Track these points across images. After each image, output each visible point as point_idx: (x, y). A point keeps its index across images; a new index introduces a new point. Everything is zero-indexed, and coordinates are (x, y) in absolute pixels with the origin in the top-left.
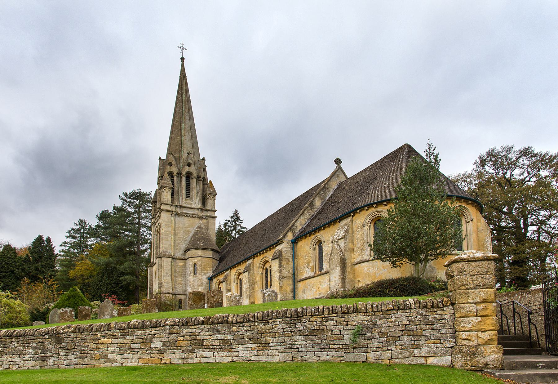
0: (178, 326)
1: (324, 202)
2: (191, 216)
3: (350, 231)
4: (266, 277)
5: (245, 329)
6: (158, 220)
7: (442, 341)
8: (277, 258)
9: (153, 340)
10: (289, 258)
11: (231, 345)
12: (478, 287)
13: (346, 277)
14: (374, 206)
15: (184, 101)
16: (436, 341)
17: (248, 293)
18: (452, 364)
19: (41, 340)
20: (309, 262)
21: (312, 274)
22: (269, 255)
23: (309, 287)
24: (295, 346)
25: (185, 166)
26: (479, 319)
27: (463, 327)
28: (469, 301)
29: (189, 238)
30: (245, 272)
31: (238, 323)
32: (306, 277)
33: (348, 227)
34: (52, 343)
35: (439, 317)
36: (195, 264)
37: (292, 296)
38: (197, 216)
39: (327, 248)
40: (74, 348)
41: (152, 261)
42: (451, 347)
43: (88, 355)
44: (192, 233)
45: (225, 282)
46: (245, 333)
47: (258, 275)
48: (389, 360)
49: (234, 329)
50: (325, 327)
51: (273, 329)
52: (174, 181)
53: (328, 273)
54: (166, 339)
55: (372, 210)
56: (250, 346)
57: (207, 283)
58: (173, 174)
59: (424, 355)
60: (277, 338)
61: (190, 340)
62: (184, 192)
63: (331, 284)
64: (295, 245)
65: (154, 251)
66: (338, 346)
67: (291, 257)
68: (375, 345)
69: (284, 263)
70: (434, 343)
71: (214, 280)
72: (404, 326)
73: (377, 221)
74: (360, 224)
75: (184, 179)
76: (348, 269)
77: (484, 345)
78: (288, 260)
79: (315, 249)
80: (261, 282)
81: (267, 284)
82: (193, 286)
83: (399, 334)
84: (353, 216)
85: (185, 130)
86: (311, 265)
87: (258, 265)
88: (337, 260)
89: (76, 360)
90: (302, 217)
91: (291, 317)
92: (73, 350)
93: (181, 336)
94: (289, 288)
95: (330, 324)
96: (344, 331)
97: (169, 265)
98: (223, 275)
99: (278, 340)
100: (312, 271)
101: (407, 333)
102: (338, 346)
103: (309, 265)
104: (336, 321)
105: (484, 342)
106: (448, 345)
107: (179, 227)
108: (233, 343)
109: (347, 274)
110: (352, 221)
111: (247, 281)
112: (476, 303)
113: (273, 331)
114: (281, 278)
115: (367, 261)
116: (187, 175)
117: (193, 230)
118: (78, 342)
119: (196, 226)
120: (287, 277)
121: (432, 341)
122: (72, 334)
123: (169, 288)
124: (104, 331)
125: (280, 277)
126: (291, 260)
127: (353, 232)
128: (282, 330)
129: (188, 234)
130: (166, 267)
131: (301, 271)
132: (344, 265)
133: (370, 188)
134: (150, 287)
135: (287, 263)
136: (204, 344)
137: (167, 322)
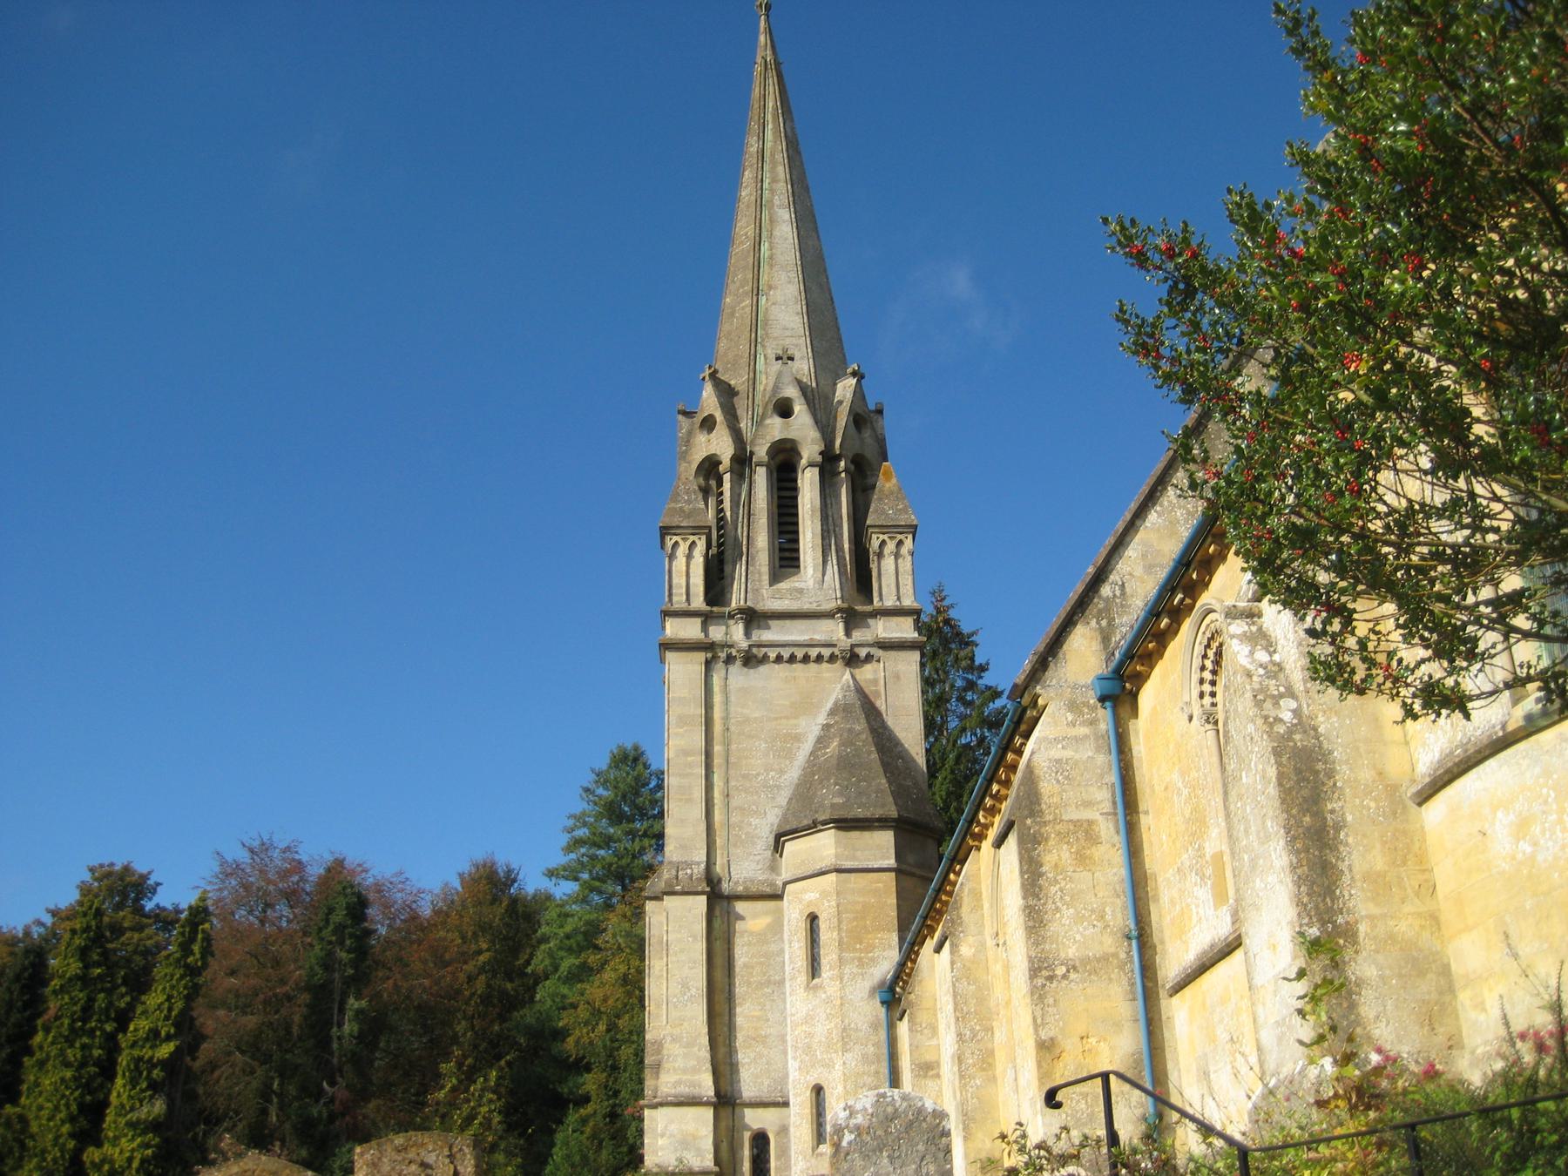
2: (800, 653)
10: (1086, 814)
13: (1350, 933)
15: (767, 154)
25: (763, 417)
29: (793, 773)
36: (813, 919)
38: (826, 652)
44: (807, 746)
57: (875, 1027)
64: (1124, 711)
67: (1107, 806)
69: (1055, 855)
75: (761, 477)
78: (1087, 831)
85: (771, 266)
90: (1153, 517)
97: (695, 937)
107: (747, 720)
109: (1359, 903)
116: (780, 457)
117: (811, 727)
119: (829, 705)
120: (1090, 966)
123: (695, 1070)
130: (682, 951)
132: (1319, 815)
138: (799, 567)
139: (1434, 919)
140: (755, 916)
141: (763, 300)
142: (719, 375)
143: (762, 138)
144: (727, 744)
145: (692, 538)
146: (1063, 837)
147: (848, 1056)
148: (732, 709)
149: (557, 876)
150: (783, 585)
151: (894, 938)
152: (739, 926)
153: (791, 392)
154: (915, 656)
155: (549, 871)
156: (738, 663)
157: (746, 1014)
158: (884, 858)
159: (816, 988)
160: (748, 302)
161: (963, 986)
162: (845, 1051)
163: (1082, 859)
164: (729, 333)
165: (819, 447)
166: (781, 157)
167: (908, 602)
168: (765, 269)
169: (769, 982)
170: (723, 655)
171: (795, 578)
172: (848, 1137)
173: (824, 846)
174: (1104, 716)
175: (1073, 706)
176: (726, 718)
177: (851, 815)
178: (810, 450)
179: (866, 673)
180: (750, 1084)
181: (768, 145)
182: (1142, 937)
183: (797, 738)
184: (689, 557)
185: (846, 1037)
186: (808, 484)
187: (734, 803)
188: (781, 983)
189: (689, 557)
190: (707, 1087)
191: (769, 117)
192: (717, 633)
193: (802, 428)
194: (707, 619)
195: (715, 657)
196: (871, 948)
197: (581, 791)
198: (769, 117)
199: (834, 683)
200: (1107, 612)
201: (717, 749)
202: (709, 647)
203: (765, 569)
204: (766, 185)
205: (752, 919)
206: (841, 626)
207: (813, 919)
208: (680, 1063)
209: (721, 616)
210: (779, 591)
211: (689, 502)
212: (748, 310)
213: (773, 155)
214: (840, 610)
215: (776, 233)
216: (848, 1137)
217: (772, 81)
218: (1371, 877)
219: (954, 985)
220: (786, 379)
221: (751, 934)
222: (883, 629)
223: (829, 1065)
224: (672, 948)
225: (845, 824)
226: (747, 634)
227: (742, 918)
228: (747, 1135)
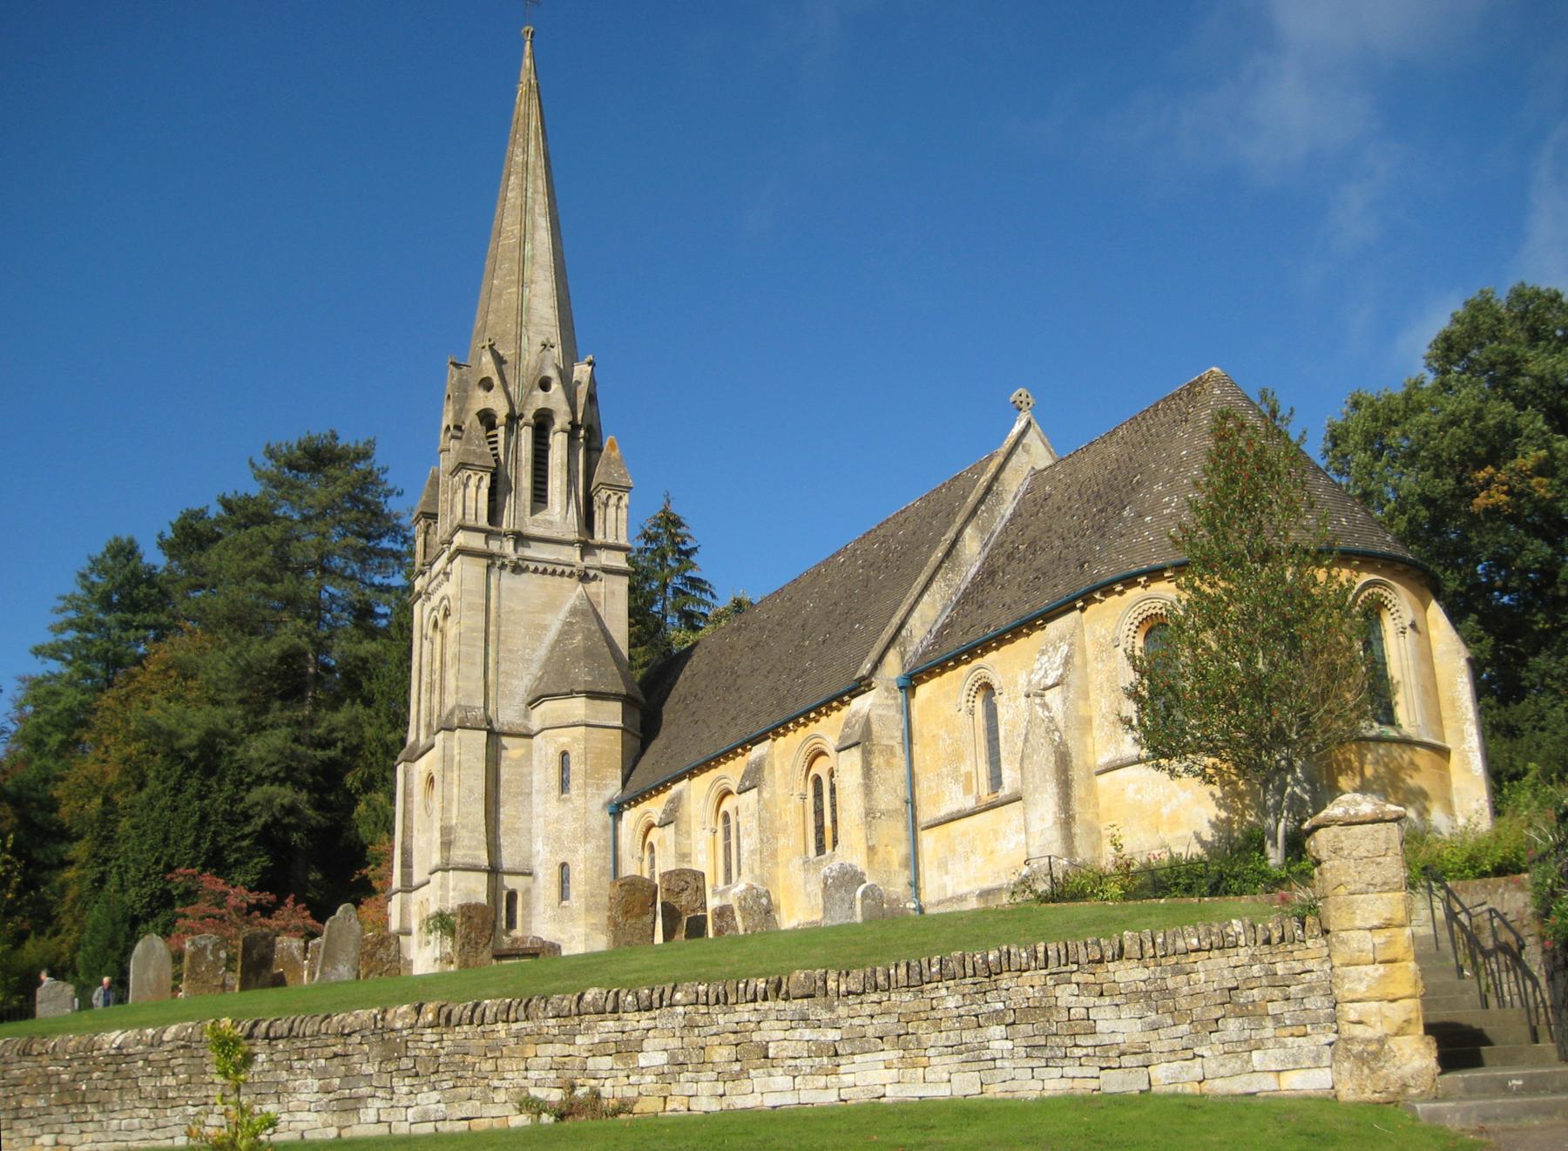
0: (707, 1004)
1: (989, 539)
2: (550, 569)
3: (1077, 660)
4: (819, 812)
5: (867, 1009)
6: (439, 585)
7: (1309, 1028)
8: (856, 744)
9: (645, 1044)
11: (836, 1054)
12: (1371, 888)
14: (1142, 580)
15: (530, 167)
16: (1296, 1031)
17: (757, 871)
18: (1333, 1088)
19: (338, 1049)
20: (957, 757)
21: (969, 803)
22: (828, 729)
23: (959, 848)
24: (987, 1055)
26: (1381, 969)
27: (1349, 989)
28: (1358, 923)
29: (542, 652)
30: (745, 791)
31: (849, 993)
32: (949, 811)
33: (1070, 645)
34: (373, 1057)
35: (1298, 967)
36: (564, 754)
37: (906, 881)
38: (568, 570)
39: (1011, 711)
40: (437, 1072)
41: (411, 738)
42: (1330, 1044)
43: (476, 1091)
44: (551, 636)
45: (672, 826)
46: (868, 1021)
47: (787, 802)
48: (1200, 1082)
49: (842, 1011)
50: (1053, 1000)
51: (933, 1009)
52: (496, 442)
53: (1020, 799)
54: (676, 1043)
55: (1135, 593)
56: (882, 1055)
57: (605, 828)
58: (495, 417)
59: (1273, 1067)
60: (944, 1034)
61: (737, 1045)
62: (526, 481)
63: (1031, 843)
65: (419, 699)
66: (1085, 1051)
67: (899, 740)
68: (1165, 1046)
69: (878, 761)
70: (1292, 1035)
71: (626, 815)
72: (1226, 992)
73: (1154, 626)
74: (1104, 637)
75: (526, 435)
76: (1078, 791)
77: (1396, 1034)
78: (891, 749)
79: (972, 713)
80: (801, 827)
81: (824, 838)
82: (559, 838)
83: (1218, 1012)
84: (1083, 609)
85: (533, 264)
86: (963, 769)
87: (788, 765)
88: (1044, 759)
89: (442, 1106)
90: (926, 597)
91: (975, 975)
92: (433, 1078)
93: (715, 1034)
94: (899, 851)
95: (1065, 995)
96: (1095, 1010)
98: (665, 797)
99: (948, 1038)
100: (967, 790)
101: (1234, 1011)
102: (1085, 1051)
103: (957, 769)
104: (1078, 984)
105: (1394, 1029)
106: (1324, 1040)
107: (512, 611)
108: (840, 1051)
109: (1076, 807)
110: (1079, 625)
111: (755, 823)
112: (1370, 929)
113: (933, 1013)
114: (870, 815)
115: (1134, 763)
116: (538, 420)
117: (555, 622)
118: (447, 1055)
119: (567, 606)
121: (1290, 1030)
122: (429, 1030)
123: (476, 848)
124: (517, 1020)
125: (867, 816)
126: (899, 750)
127: (1085, 664)
128: (956, 1012)
131: (930, 788)
132: (1067, 776)
133: (1125, 513)
134: (403, 843)
135: (888, 763)
136: (770, 1055)
137: (678, 996)
138: (546, 503)
139: (1098, 814)
140: (514, 748)
141: (527, 291)
142: (496, 347)
143: (526, 151)
144: (498, 626)
145: (481, 474)
146: (881, 752)
147: (588, 846)
148: (503, 602)
149: (44, 655)
150: (538, 516)
151: (619, 773)
152: (504, 753)
153: (551, 373)
154: (625, 581)
155: (37, 649)
156: (508, 569)
157: (506, 812)
158: (615, 720)
159: (565, 801)
160: (514, 290)
161: (764, 814)
162: (586, 842)
163: (888, 763)
164: (498, 310)
165: (569, 418)
166: (541, 172)
167: (623, 541)
168: (528, 264)
169: (521, 794)
170: (498, 563)
171: (545, 512)
172: (830, 881)
173: (578, 707)
174: (900, 696)
175: (887, 689)
176: (498, 608)
177: (597, 690)
178: (561, 420)
179: (593, 587)
180: (507, 860)
181: (531, 160)
182: (911, 802)
183: (545, 628)
184: (478, 487)
185: (587, 833)
186: (558, 444)
187: (502, 668)
188: (530, 794)
189: (478, 487)
190: (483, 859)
191: (532, 134)
192: (494, 546)
193: (555, 398)
194: (489, 535)
195: (493, 564)
196: (605, 778)
197: (76, 575)
198: (532, 134)
199: (572, 593)
200: (903, 644)
201: (492, 629)
202: (490, 556)
203: (528, 504)
204: (529, 194)
205: (513, 749)
206: (578, 553)
207: (564, 754)
208: (466, 842)
209: (499, 534)
210: (536, 521)
211: (479, 446)
212: (515, 296)
213: (534, 169)
214: (579, 542)
215: (537, 237)
216: (830, 881)
217: (535, 102)
218: (1080, 799)
219: (1484, 874)
220: (548, 362)
221: (512, 760)
222: (605, 558)
223: (575, 851)
224: (464, 765)
225: (593, 695)
226: (516, 550)
227: (506, 749)
228: (505, 893)
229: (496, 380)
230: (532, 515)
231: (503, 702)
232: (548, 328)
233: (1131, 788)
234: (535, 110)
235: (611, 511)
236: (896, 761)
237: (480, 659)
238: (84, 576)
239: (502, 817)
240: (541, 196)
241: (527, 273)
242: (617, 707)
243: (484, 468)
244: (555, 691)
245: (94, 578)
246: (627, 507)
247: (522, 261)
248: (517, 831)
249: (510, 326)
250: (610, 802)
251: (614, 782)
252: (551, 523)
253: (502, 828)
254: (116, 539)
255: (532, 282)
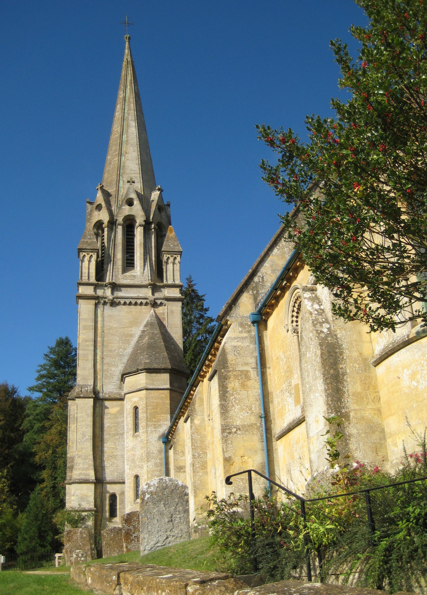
10: (245, 368)
13: (347, 416)
15: (127, 98)
25: (122, 206)
38: (144, 301)
57: (160, 452)
62: (119, 255)
64: (262, 327)
67: (254, 365)
75: (120, 230)
78: (246, 375)
85: (127, 144)
90: (275, 251)
116: (128, 222)
117: (137, 331)
119: (145, 323)
123: (87, 469)
129: (128, 342)
130: (83, 421)
138: (134, 267)
139: (379, 411)
140: (113, 407)
141: (123, 158)
143: (125, 92)
144: (103, 337)
145: (91, 254)
147: (149, 463)
152: (106, 411)
153: (133, 196)
155: (30, 388)
156: (108, 305)
157: (108, 446)
158: (165, 384)
159: (137, 436)
162: (148, 461)
165: (144, 218)
167: (178, 282)
169: (118, 434)
170: (102, 301)
171: (132, 271)
172: (147, 496)
174: (254, 329)
175: (241, 325)
176: (103, 327)
178: (140, 219)
179: (160, 310)
181: (128, 95)
183: (132, 336)
184: (90, 261)
185: (149, 456)
186: (139, 233)
187: (105, 361)
188: (123, 434)
189: (90, 261)
190: (92, 476)
192: (100, 292)
194: (96, 287)
196: (159, 420)
198: (128, 84)
200: (256, 288)
201: (99, 339)
202: (96, 298)
203: (120, 267)
204: (126, 111)
208: (81, 466)
210: (125, 276)
212: (117, 162)
213: (129, 99)
214: (150, 285)
215: (129, 131)
220: (131, 190)
221: (111, 414)
222: (167, 293)
223: (141, 467)
225: (150, 371)
226: (112, 293)
227: (107, 408)
228: (108, 495)
229: (103, 204)
230: (123, 273)
231: (106, 381)
232: (135, 175)
233: (406, 375)
234: (130, 72)
235: (170, 266)
236: (250, 383)
237: (91, 357)
238: (46, 355)
239: (105, 449)
240: (133, 111)
241: (124, 149)
242: (166, 377)
243: (93, 250)
244: (129, 371)
245: (52, 356)
246: (180, 263)
247: (121, 144)
248: (115, 457)
249: (115, 177)
250: (163, 435)
251: (165, 423)
252: (134, 276)
253: (106, 456)
254: (60, 338)
255: (126, 153)
